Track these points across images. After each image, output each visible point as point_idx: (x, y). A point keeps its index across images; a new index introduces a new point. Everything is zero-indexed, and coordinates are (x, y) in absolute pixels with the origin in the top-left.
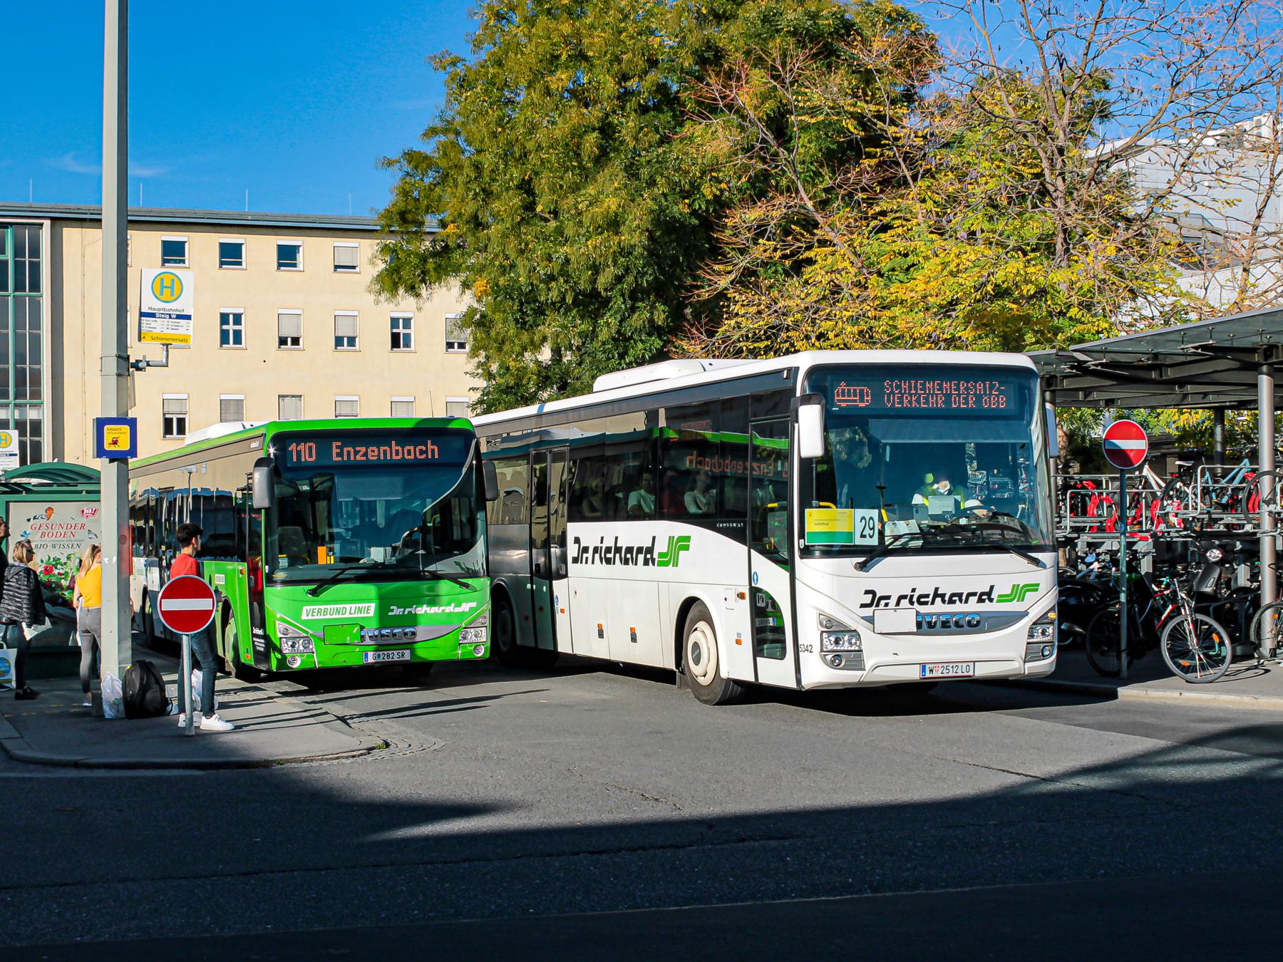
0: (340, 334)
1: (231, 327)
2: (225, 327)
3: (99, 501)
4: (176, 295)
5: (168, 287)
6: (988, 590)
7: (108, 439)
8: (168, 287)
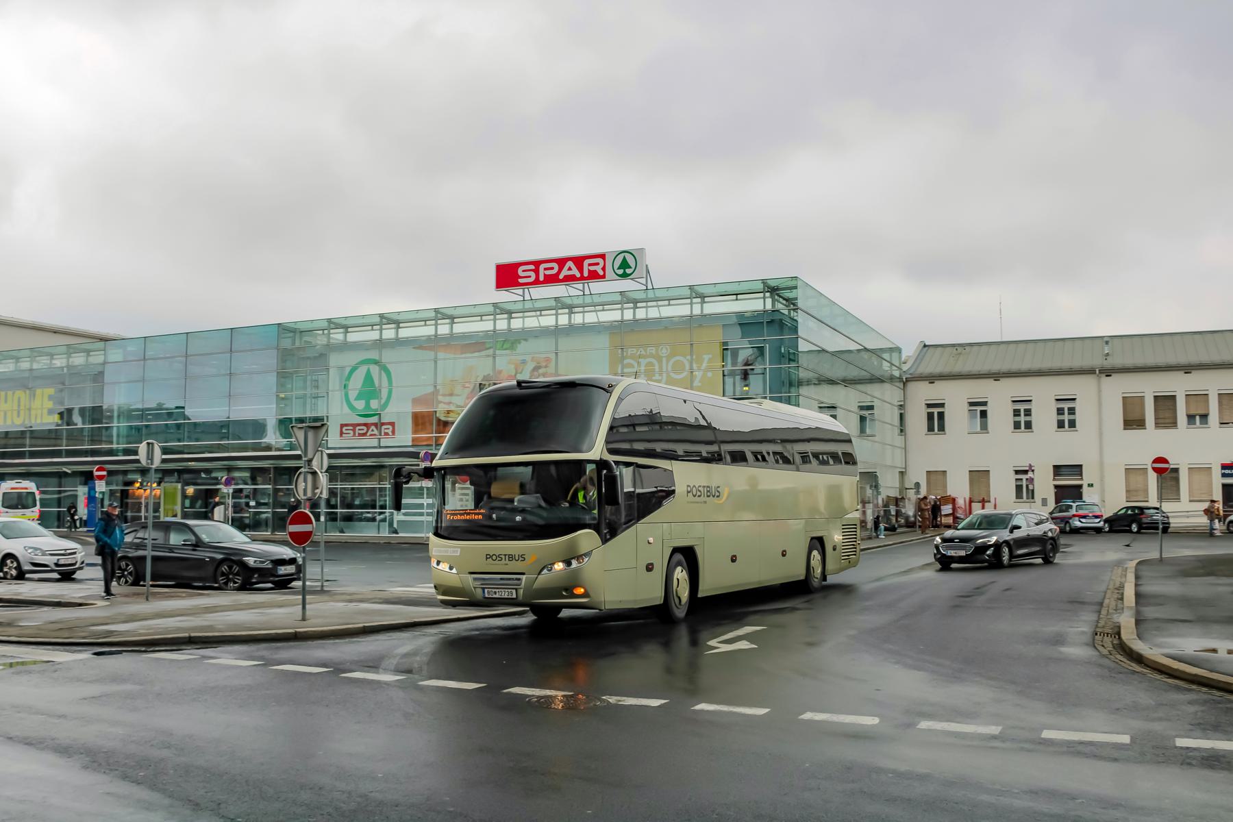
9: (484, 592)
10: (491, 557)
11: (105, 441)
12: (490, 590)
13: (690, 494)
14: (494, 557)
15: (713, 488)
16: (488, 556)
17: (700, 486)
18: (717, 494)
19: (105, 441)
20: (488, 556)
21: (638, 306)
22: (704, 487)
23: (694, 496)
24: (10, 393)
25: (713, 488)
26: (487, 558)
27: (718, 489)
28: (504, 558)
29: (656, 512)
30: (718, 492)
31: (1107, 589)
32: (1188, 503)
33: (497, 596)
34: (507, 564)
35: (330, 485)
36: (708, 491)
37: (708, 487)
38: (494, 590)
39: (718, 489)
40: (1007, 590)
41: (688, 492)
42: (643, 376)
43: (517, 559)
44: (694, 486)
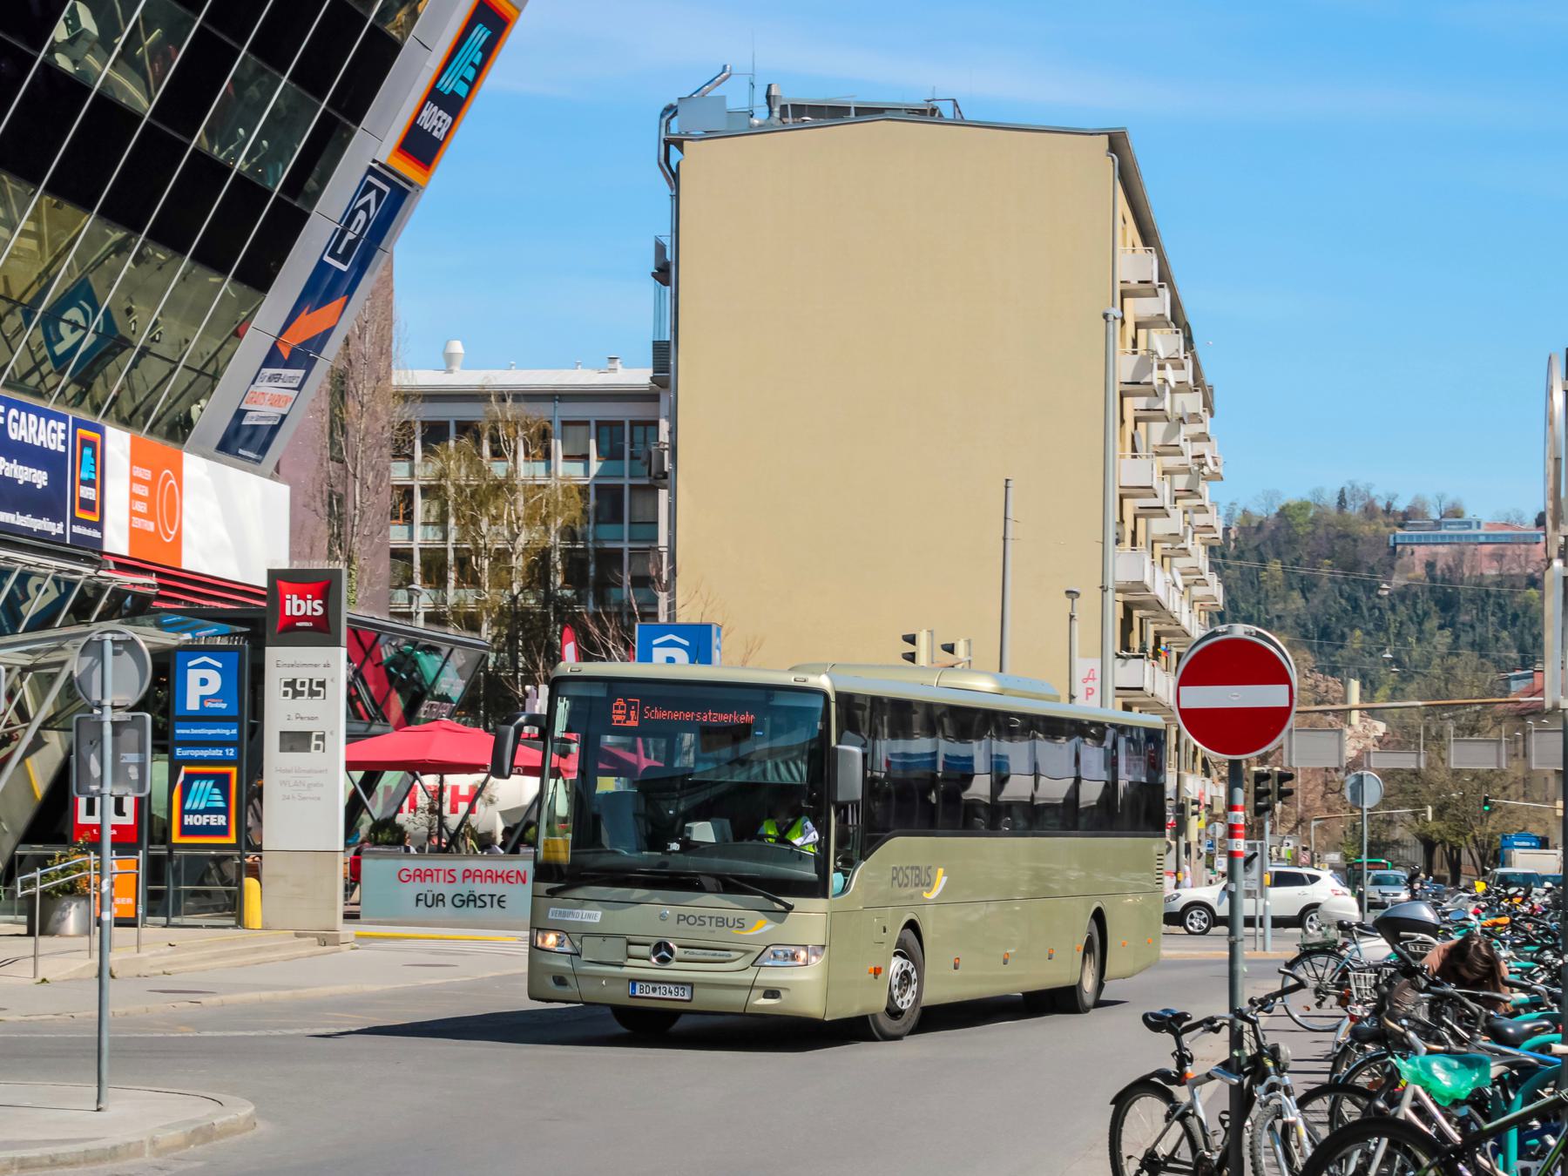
7: (425, 113)
9: (634, 988)
10: (686, 919)
11: (190, 271)
13: (896, 882)
14: (692, 920)
16: (682, 918)
17: (907, 868)
19: (190, 271)
21: (1327, 1076)
22: (912, 868)
23: (900, 886)
24: (485, 29)
26: (678, 920)
27: (452, 873)
28: (708, 924)
29: (358, 289)
31: (1355, 540)
32: (1143, 1013)
33: (656, 995)
34: (714, 932)
35: (883, 736)
36: (917, 876)
37: (918, 868)
39: (452, 873)
41: (894, 879)
42: (1285, 1119)
44: (901, 868)
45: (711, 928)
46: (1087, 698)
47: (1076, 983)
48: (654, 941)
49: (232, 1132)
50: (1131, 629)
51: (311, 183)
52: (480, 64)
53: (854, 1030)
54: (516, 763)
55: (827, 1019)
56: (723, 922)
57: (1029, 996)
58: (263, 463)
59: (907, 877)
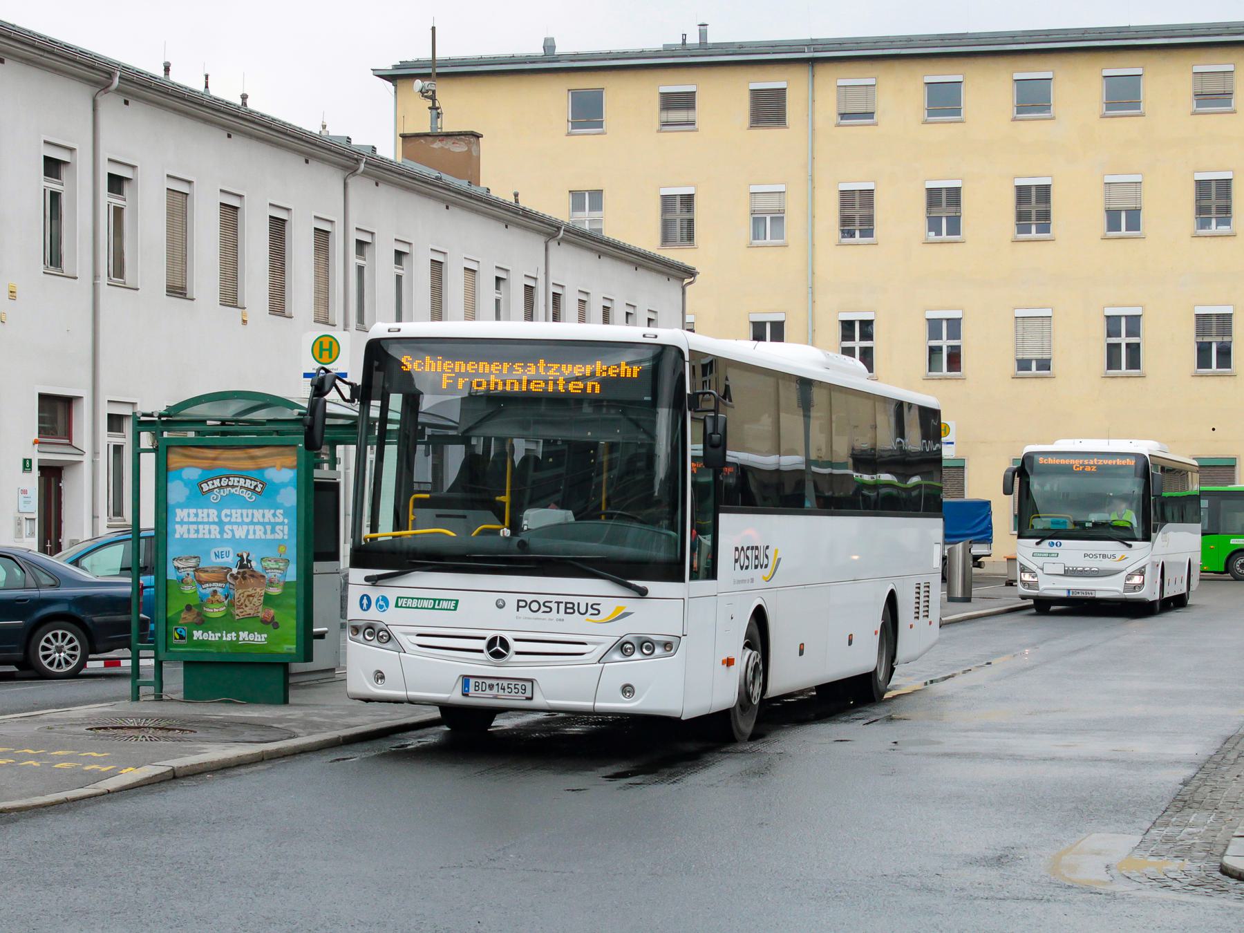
0: (1113, 206)
1: (1123, 340)
2: (669, 216)
3: (498, 318)
4: (333, 358)
5: (327, 350)
6: (73, 444)
8: (327, 350)
9: (1069, 592)
10: (528, 605)
12: (480, 681)
13: (738, 564)
15: (762, 548)
16: (522, 604)
18: (766, 562)
20: (522, 604)
22: (752, 548)
23: (742, 568)
25: (762, 548)
26: (519, 607)
30: (767, 557)
36: (756, 557)
38: (488, 682)
40: (560, 620)
41: (736, 561)
43: (582, 610)
45: (559, 616)
46: (518, 610)
47: (872, 669)
48: (490, 635)
49: (1066, 471)
50: (319, 717)
51: (58, 73)
52: (157, 529)
53: (1032, 668)
54: (428, 130)
55: (683, 718)
56: (573, 608)
57: (824, 689)
58: (29, 458)
59: (748, 558)
